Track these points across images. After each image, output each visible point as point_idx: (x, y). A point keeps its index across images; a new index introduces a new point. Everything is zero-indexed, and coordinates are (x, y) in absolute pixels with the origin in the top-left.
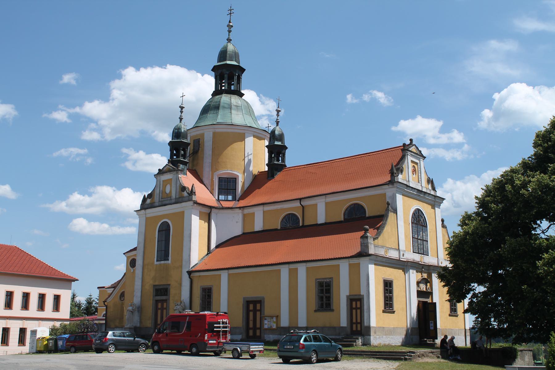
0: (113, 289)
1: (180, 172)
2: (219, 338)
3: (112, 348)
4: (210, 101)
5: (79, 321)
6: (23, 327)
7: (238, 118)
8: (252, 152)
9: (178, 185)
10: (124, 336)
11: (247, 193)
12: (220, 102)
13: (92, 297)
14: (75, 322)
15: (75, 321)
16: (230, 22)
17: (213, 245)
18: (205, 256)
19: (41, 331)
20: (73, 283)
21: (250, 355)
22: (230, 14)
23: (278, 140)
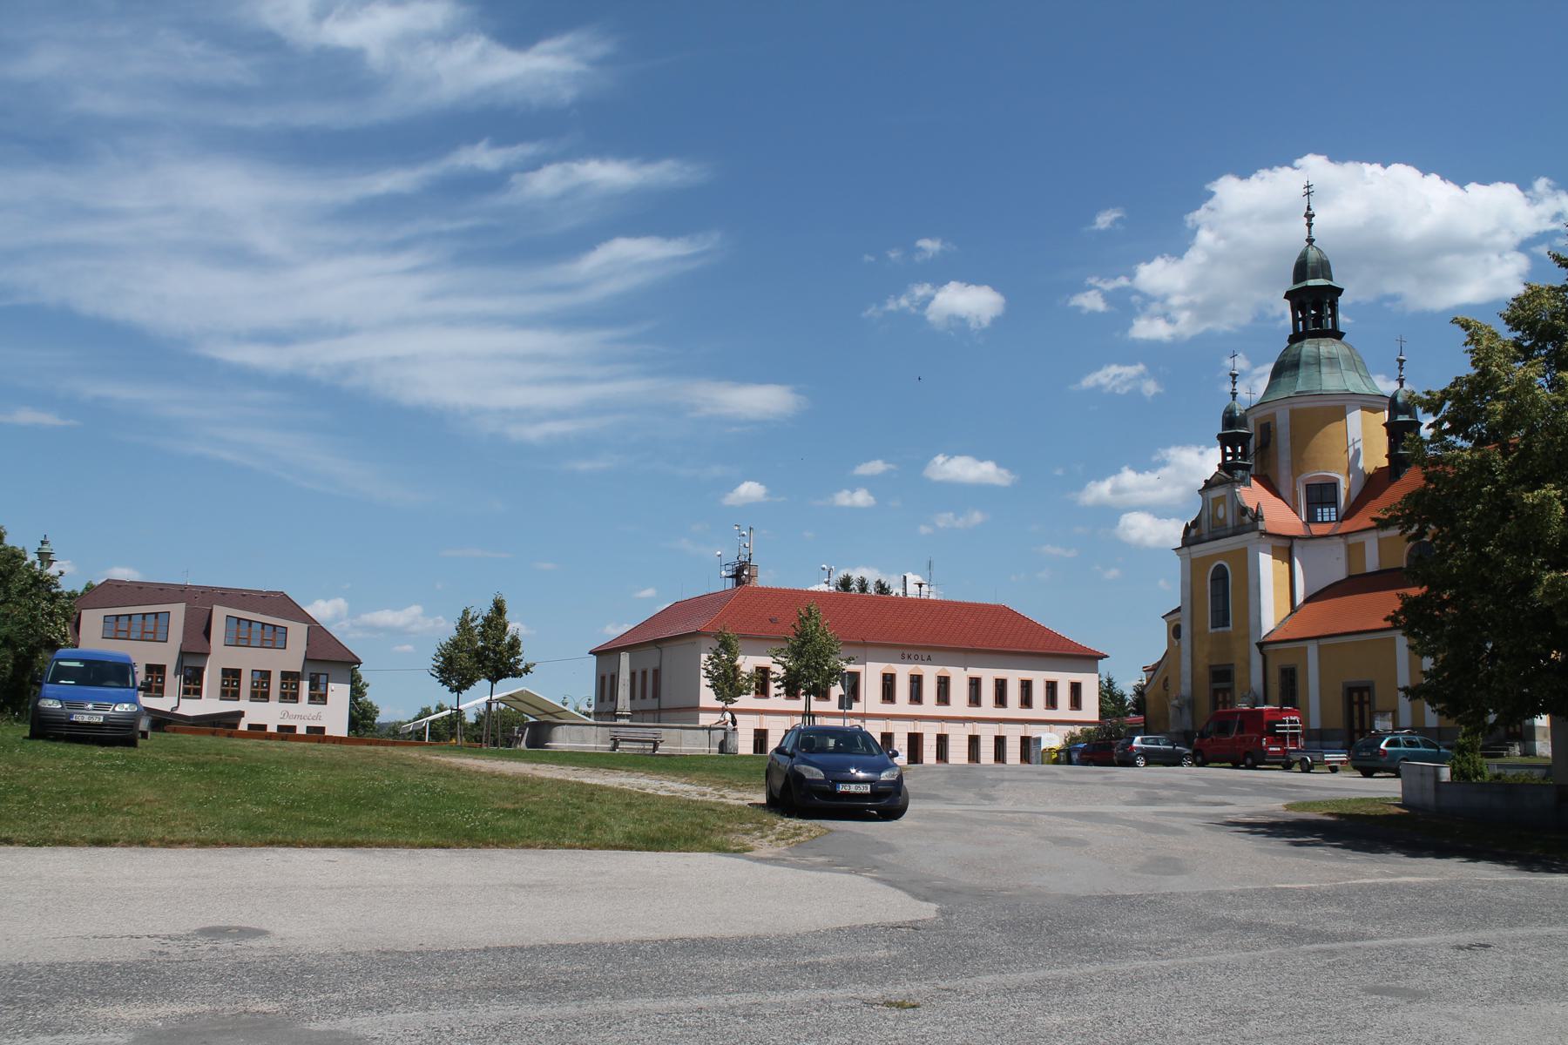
0: (1152, 672)
1: (1236, 484)
2: (1285, 744)
3: (1141, 761)
4: (1284, 354)
7: (1332, 382)
8: (1360, 437)
9: (1235, 506)
11: (1354, 508)
12: (1299, 354)
16: (1309, 208)
17: (1299, 599)
18: (1287, 617)
20: (1099, 661)
21: (1330, 768)
22: (1308, 193)
23: (1403, 413)
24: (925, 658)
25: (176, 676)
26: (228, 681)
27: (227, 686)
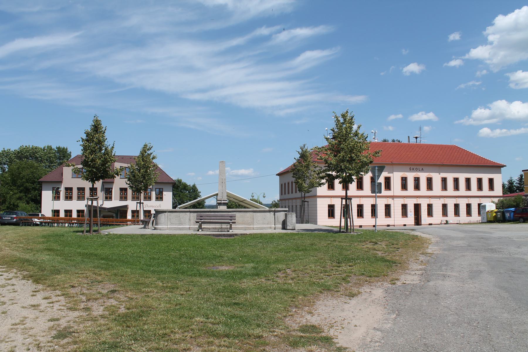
5: (513, 197)
6: (405, 203)
10: (28, 222)
13: (512, 179)
14: (510, 198)
15: (510, 197)
19: (489, 206)
24: (421, 169)
25: (101, 192)
26: (122, 193)
27: (122, 195)
